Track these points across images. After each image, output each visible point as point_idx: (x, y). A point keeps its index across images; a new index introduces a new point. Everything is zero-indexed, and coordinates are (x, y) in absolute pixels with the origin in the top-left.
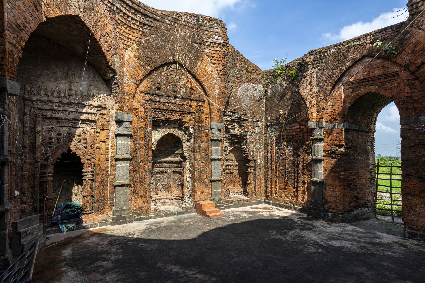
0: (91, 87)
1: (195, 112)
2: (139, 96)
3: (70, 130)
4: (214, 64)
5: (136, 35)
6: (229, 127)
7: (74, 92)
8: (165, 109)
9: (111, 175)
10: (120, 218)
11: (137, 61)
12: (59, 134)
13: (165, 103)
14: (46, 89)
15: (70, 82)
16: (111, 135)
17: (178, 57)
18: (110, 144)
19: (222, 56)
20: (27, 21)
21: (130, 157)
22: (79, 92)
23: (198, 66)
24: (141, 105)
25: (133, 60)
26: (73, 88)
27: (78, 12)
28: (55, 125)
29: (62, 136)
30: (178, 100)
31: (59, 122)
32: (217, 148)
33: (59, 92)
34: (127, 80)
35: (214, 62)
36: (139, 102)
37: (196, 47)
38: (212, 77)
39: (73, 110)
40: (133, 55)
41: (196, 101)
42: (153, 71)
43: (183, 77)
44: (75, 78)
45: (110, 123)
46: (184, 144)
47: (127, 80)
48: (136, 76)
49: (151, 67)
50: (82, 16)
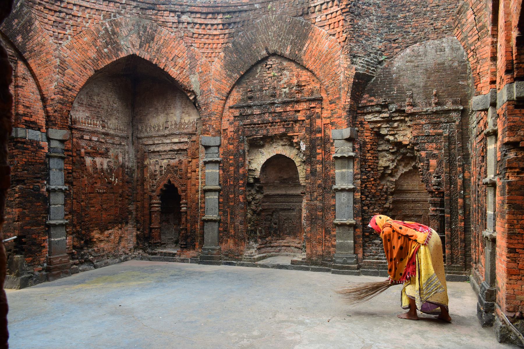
0: (183, 114)
1: (304, 118)
2: (228, 113)
3: (169, 161)
4: (334, 35)
5: (222, 41)
6: (383, 132)
7: (169, 123)
8: (260, 122)
9: (201, 208)
10: (208, 258)
11: (223, 72)
12: (161, 167)
13: (260, 114)
14: (151, 126)
15: (167, 114)
16: (201, 163)
17: (274, 47)
18: (200, 174)
19: (341, 17)
20: (75, 81)
21: (218, 187)
22: (173, 123)
23: (305, 49)
24: (231, 124)
25: (220, 72)
26: (169, 119)
27: (132, 51)
28: (158, 158)
29: (163, 168)
30: (277, 107)
31: (160, 155)
32: (344, 170)
33: (159, 126)
34: (214, 97)
35: (332, 32)
36: (229, 120)
37: (300, 21)
38: (331, 58)
39: (168, 141)
40: (219, 65)
41: (305, 102)
42: (242, 77)
43: (285, 72)
44: (171, 109)
45: (200, 150)
46: (299, 168)
47: (214, 97)
48: (223, 90)
49: (239, 73)
50: (137, 53)
